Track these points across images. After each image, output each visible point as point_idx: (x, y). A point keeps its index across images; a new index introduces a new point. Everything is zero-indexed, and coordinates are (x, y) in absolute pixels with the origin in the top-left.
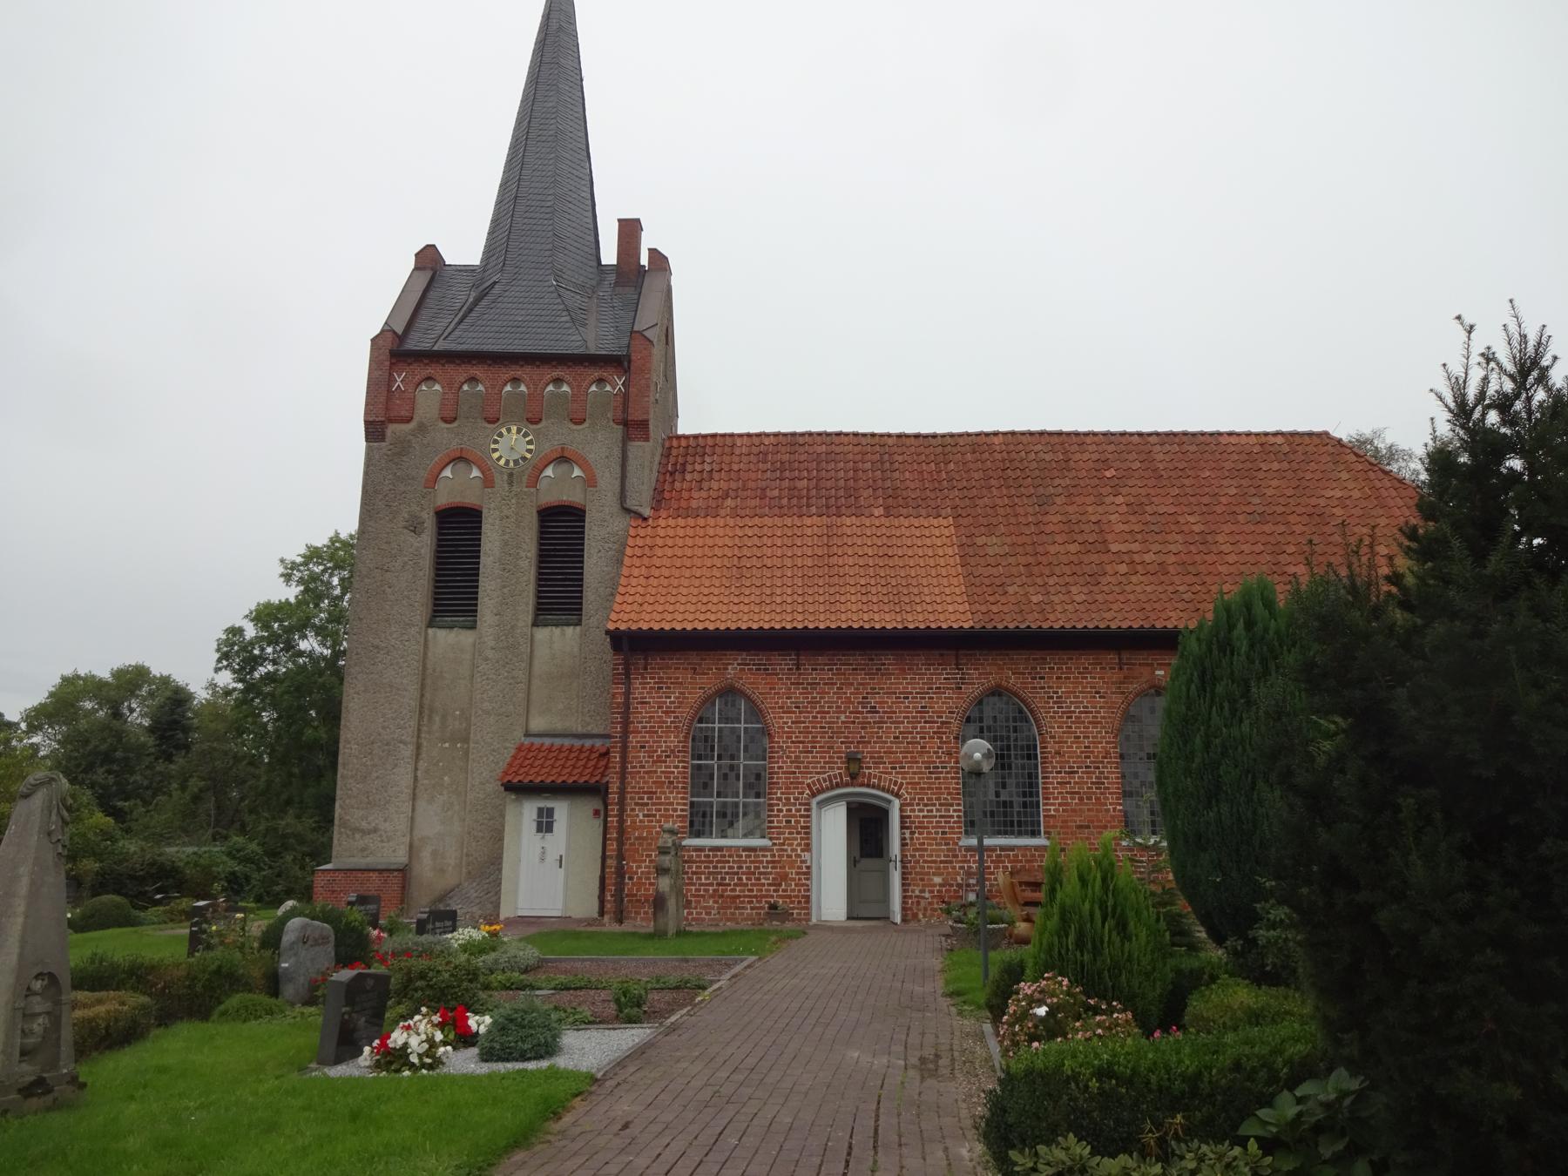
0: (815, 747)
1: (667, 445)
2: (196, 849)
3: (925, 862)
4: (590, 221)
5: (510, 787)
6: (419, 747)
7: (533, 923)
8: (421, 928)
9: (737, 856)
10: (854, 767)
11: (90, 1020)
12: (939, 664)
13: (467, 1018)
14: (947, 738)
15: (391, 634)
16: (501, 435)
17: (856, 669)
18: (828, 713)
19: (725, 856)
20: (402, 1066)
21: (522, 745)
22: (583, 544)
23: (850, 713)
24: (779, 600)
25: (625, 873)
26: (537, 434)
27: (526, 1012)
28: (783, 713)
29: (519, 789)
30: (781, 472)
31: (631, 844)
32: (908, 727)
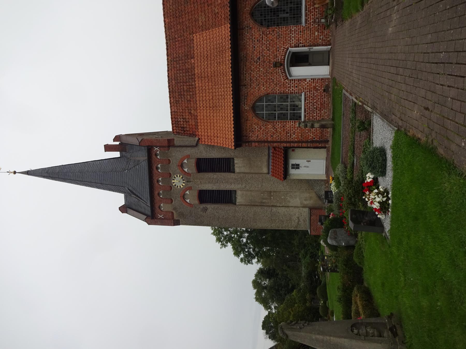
0: (272, 78)
1: (175, 133)
2: (303, 267)
3: (310, 38)
4: (106, 160)
5: (285, 178)
6: (273, 206)
7: (328, 169)
8: (331, 202)
9: (307, 103)
10: (278, 65)
11: (363, 306)
12: (243, 36)
13: (367, 182)
14: (268, 32)
15: (238, 215)
16: (175, 185)
17: (245, 65)
18: (260, 74)
19: (307, 108)
20: (387, 204)
21: (272, 175)
22: (208, 158)
23: (260, 67)
24: (223, 93)
25: (313, 140)
26: (174, 174)
27: (368, 160)
28: (260, 90)
29: (286, 175)
30: (182, 95)
31: (303, 139)
32: (265, 46)
